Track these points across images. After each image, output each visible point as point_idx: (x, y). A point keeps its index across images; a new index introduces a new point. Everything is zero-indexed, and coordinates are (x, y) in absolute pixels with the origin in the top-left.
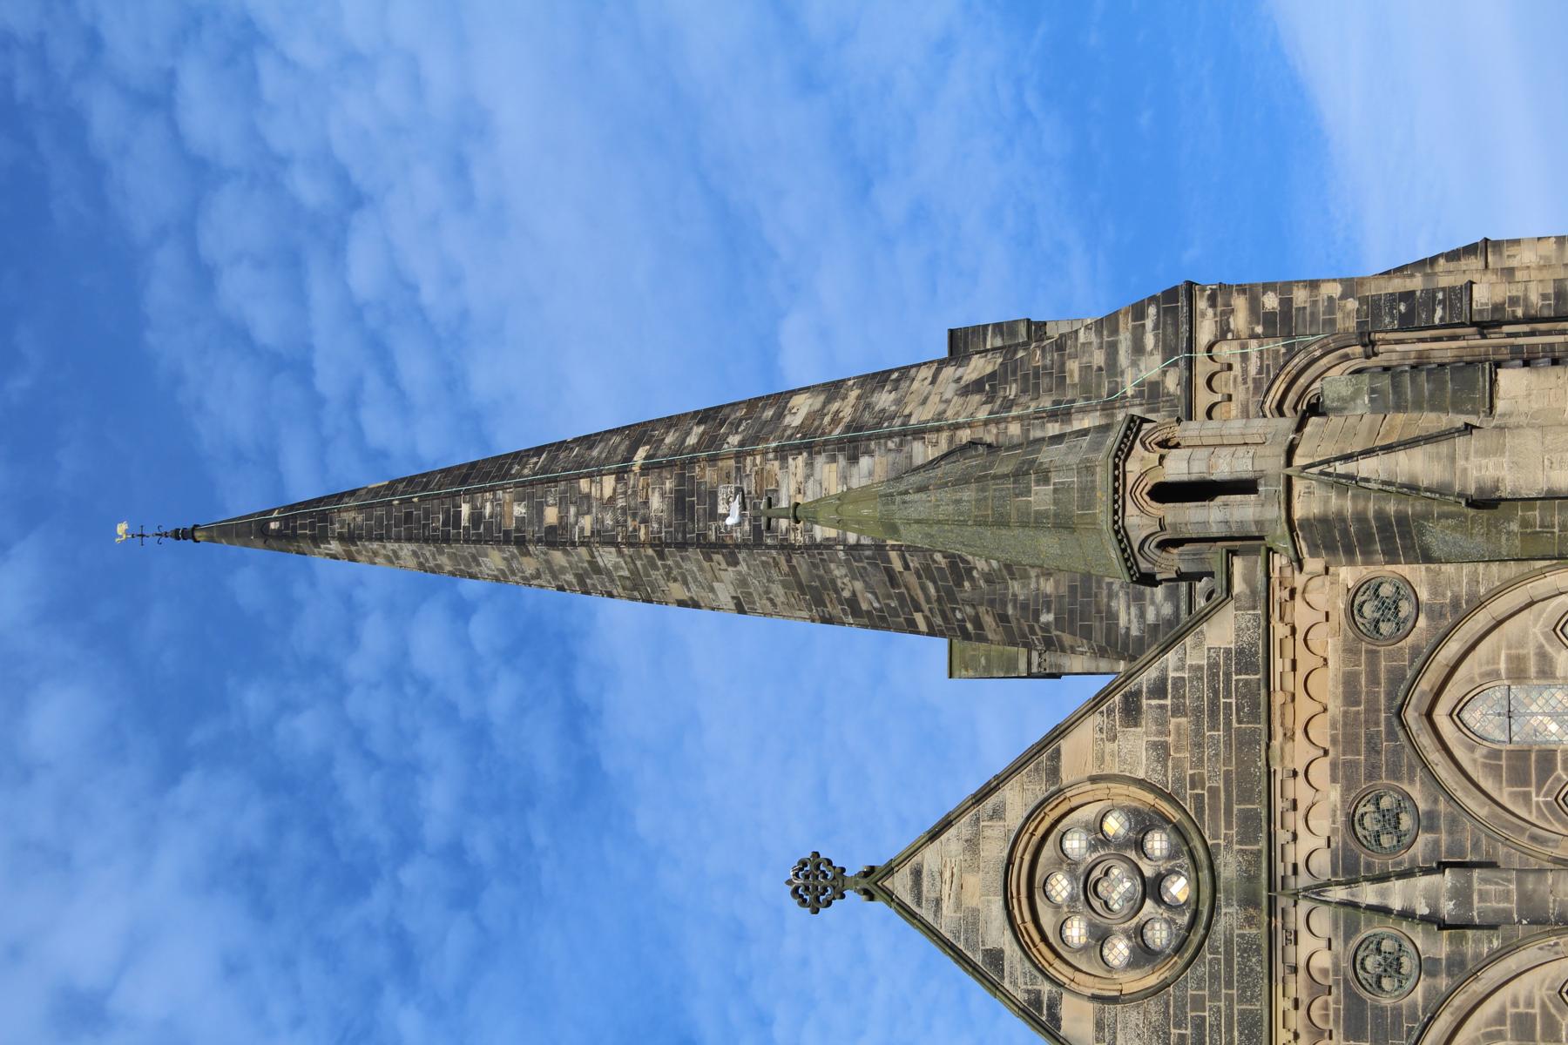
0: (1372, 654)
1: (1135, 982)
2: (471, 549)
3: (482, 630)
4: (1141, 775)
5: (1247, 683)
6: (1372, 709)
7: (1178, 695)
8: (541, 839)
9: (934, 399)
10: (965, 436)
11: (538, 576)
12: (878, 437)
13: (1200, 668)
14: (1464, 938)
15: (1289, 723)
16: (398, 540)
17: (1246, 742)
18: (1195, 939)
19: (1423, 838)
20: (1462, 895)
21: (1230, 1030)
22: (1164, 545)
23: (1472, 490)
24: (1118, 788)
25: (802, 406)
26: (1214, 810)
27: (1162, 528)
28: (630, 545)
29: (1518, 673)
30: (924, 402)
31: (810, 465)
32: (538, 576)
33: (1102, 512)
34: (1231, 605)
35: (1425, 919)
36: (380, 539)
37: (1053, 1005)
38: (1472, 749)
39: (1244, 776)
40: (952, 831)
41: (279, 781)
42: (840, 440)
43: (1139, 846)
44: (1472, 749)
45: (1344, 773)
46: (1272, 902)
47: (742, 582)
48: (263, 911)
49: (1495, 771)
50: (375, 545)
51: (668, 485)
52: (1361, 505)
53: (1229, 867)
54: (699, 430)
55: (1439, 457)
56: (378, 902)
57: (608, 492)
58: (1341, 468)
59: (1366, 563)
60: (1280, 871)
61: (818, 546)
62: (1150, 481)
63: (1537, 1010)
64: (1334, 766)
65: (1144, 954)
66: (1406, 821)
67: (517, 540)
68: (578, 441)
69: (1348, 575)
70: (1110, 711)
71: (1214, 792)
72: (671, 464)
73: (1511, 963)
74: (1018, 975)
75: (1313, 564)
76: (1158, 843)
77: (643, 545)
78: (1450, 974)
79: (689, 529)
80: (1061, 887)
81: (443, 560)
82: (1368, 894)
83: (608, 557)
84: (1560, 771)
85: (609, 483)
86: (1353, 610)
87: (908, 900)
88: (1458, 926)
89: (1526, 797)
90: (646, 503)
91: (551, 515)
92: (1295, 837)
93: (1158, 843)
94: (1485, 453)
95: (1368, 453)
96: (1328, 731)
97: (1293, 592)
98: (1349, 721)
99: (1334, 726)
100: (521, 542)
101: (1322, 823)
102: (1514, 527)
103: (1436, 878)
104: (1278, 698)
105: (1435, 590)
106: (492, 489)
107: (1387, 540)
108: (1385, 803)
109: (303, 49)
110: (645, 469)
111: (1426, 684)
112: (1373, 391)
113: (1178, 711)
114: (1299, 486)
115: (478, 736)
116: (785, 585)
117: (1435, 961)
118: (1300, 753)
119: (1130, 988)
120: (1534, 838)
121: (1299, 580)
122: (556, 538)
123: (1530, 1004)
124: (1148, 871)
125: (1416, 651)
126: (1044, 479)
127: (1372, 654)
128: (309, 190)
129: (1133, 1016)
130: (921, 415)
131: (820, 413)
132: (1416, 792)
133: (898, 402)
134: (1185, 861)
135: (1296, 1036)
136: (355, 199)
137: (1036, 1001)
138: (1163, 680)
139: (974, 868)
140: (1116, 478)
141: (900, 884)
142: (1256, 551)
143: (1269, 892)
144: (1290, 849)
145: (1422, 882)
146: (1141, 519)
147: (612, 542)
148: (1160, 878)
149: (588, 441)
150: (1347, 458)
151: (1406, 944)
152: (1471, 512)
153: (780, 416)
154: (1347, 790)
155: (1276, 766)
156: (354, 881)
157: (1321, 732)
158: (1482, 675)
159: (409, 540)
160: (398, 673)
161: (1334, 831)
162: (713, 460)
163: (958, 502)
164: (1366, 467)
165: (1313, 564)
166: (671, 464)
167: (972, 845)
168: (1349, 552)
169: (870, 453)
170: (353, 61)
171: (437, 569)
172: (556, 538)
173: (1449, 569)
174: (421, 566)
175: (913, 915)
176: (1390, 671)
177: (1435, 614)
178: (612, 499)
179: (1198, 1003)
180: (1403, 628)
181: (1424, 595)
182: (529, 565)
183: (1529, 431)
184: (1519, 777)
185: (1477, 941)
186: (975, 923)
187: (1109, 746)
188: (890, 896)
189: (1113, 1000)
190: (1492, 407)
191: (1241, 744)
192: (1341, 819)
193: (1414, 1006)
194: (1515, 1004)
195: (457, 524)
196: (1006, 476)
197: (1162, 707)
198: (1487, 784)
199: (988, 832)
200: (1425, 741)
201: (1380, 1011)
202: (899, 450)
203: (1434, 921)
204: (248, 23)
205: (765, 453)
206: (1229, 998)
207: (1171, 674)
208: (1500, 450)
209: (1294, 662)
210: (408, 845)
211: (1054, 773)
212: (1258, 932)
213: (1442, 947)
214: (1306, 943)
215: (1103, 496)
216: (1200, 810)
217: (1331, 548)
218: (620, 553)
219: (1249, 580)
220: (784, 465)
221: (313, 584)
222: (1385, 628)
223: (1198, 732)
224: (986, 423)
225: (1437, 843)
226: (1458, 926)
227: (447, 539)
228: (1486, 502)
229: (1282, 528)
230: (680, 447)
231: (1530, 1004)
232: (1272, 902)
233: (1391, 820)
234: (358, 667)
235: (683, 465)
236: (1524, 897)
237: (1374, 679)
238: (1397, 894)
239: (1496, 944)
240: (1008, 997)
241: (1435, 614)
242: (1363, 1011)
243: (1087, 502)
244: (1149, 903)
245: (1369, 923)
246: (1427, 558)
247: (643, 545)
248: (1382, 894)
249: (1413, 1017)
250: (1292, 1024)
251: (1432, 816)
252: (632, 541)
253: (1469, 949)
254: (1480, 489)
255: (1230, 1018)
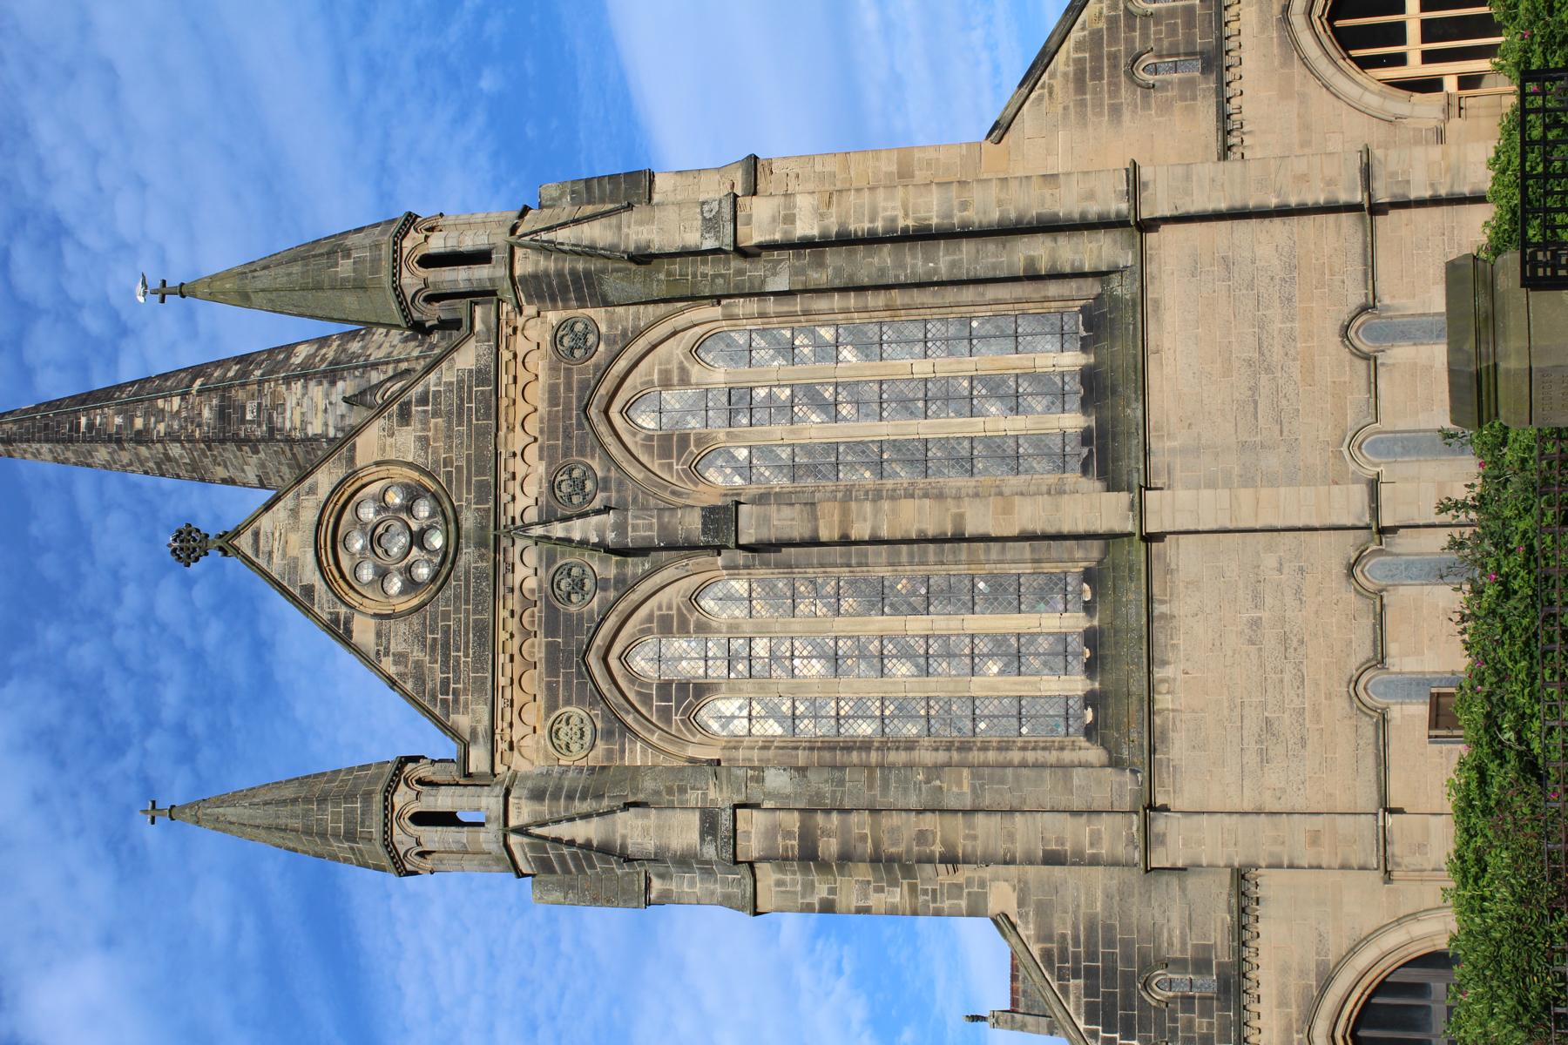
0: (568, 371)
1: (404, 604)
2: (87, 446)
3: (202, 595)
4: (410, 459)
5: (483, 392)
6: (568, 409)
7: (437, 403)
8: (236, 721)
9: (386, 345)
10: (404, 366)
11: (131, 464)
12: (349, 369)
13: (451, 383)
14: (626, 563)
15: (511, 420)
16: (39, 441)
17: (481, 433)
18: (444, 572)
19: (600, 496)
20: (621, 528)
21: (467, 634)
22: (430, 299)
23: (632, 248)
24: (396, 471)
25: (302, 352)
26: (459, 481)
27: (426, 286)
28: (189, 441)
29: (666, 384)
30: (380, 347)
31: (305, 387)
32: (131, 464)
33: (385, 277)
34: (473, 341)
35: (596, 547)
36: (28, 441)
37: (348, 621)
38: (634, 435)
39: (480, 457)
40: (281, 504)
41: (68, 684)
42: (324, 371)
43: (409, 510)
44: (634, 435)
45: (547, 454)
46: (497, 539)
47: (262, 465)
48: (60, 764)
49: (649, 449)
50: (25, 446)
51: (215, 402)
52: (560, 265)
53: (468, 521)
54: (236, 368)
55: (610, 226)
56: (130, 760)
57: (175, 408)
58: (545, 236)
59: (565, 308)
60: (503, 522)
61: (309, 439)
62: (419, 253)
63: (674, 612)
64: (541, 449)
65: (411, 585)
66: (589, 485)
67: (117, 440)
68: (158, 377)
69: (553, 317)
70: (390, 416)
71: (459, 469)
72: (216, 389)
73: (657, 579)
74: (324, 603)
75: (529, 310)
76: (423, 509)
77: (198, 441)
78: (616, 589)
79: (228, 431)
80: (357, 544)
81: (69, 454)
82: (558, 530)
83: (175, 450)
84: (692, 448)
85: (176, 401)
86: (556, 341)
87: (250, 553)
88: (623, 552)
89: (670, 466)
90: (200, 414)
91: (139, 423)
92: (514, 498)
93: (423, 509)
94: (641, 223)
95: (563, 225)
96: (538, 425)
97: (515, 329)
98: (552, 418)
99: (541, 421)
100: (119, 441)
101: (532, 489)
102: (662, 276)
103: (603, 517)
104: (504, 402)
105: (611, 326)
106: (101, 407)
107: (579, 290)
108: (576, 474)
109: (91, 238)
110: (200, 392)
111: (603, 390)
112: (573, 192)
113: (436, 414)
114: (519, 252)
115: (197, 658)
116: (290, 466)
117: (606, 580)
118: (518, 440)
119: (399, 608)
120: (673, 493)
121: (520, 321)
122: (142, 438)
123: (670, 608)
124: (415, 527)
125: (597, 367)
126: (347, 253)
127: (568, 371)
128: (94, 324)
129: (401, 627)
130: (376, 355)
131: (314, 355)
132: (595, 464)
133: (363, 348)
134: (439, 519)
135: (512, 636)
136: (123, 330)
137: (336, 620)
138: (426, 393)
139: (295, 529)
140: (395, 252)
141: (244, 542)
142: (491, 302)
143: (497, 536)
144: (510, 507)
145: (595, 519)
146: (412, 279)
147: (178, 440)
148: (423, 532)
149: (165, 377)
150: (549, 229)
151: (587, 569)
152: (633, 267)
153: (288, 358)
154: (549, 465)
155: (502, 449)
156: (115, 749)
157: (533, 426)
158: (642, 384)
159: (47, 441)
160: (147, 618)
161: (541, 493)
162: (243, 385)
163: (289, 274)
164: (562, 235)
165: (529, 310)
166: (216, 389)
167: (294, 513)
168: (553, 300)
169: (344, 379)
170: (124, 248)
171: (66, 461)
172: (142, 438)
173: (620, 310)
174: (55, 459)
175: (253, 563)
176: (580, 382)
177: (611, 341)
178: (178, 412)
179: (446, 615)
180: (590, 352)
181: (603, 329)
182: (125, 457)
183: (671, 208)
184: (665, 453)
185: (635, 565)
186: (296, 567)
187: (389, 440)
188: (237, 550)
189: (388, 617)
190: (650, 199)
191: (478, 434)
192: (545, 485)
193: (591, 612)
194: (660, 608)
195: (78, 430)
196: (322, 255)
197: (425, 412)
198: (644, 459)
199: (305, 504)
200: (603, 429)
201: (569, 616)
202: (362, 376)
203: (603, 548)
204: (56, 221)
205: (276, 380)
206: (467, 611)
207: (432, 389)
208: (651, 221)
209: (515, 378)
210: (151, 723)
211: (351, 460)
212: (487, 565)
213: (609, 569)
214: (520, 571)
215: (386, 265)
216: (449, 482)
217: (541, 298)
218: (183, 447)
219: (485, 322)
220: (289, 388)
221: (93, 563)
222: (577, 353)
223: (449, 428)
224: (417, 358)
225: (609, 498)
226: (623, 552)
227: (71, 440)
228: (643, 258)
229: (507, 284)
230: (223, 378)
231: (670, 608)
232: (497, 539)
233: (579, 485)
234: (121, 616)
235: (224, 389)
236: (663, 527)
237: (569, 388)
238: (577, 529)
239: (647, 566)
240: (316, 617)
241: (611, 341)
242: (557, 617)
243: (375, 270)
244: (415, 550)
245: (563, 555)
246: (606, 303)
247: (198, 441)
248: (567, 530)
249: (591, 619)
250: (509, 629)
251: (606, 480)
252: (191, 439)
253: (629, 571)
254: (637, 248)
255: (467, 625)
